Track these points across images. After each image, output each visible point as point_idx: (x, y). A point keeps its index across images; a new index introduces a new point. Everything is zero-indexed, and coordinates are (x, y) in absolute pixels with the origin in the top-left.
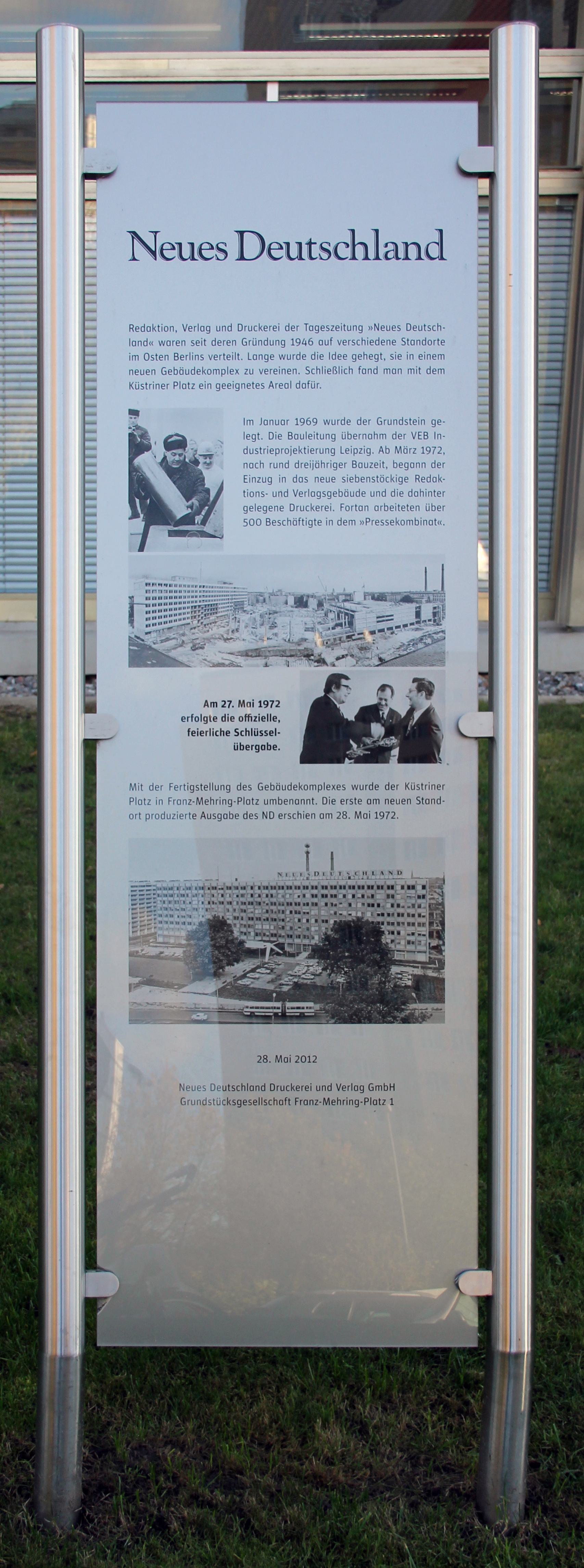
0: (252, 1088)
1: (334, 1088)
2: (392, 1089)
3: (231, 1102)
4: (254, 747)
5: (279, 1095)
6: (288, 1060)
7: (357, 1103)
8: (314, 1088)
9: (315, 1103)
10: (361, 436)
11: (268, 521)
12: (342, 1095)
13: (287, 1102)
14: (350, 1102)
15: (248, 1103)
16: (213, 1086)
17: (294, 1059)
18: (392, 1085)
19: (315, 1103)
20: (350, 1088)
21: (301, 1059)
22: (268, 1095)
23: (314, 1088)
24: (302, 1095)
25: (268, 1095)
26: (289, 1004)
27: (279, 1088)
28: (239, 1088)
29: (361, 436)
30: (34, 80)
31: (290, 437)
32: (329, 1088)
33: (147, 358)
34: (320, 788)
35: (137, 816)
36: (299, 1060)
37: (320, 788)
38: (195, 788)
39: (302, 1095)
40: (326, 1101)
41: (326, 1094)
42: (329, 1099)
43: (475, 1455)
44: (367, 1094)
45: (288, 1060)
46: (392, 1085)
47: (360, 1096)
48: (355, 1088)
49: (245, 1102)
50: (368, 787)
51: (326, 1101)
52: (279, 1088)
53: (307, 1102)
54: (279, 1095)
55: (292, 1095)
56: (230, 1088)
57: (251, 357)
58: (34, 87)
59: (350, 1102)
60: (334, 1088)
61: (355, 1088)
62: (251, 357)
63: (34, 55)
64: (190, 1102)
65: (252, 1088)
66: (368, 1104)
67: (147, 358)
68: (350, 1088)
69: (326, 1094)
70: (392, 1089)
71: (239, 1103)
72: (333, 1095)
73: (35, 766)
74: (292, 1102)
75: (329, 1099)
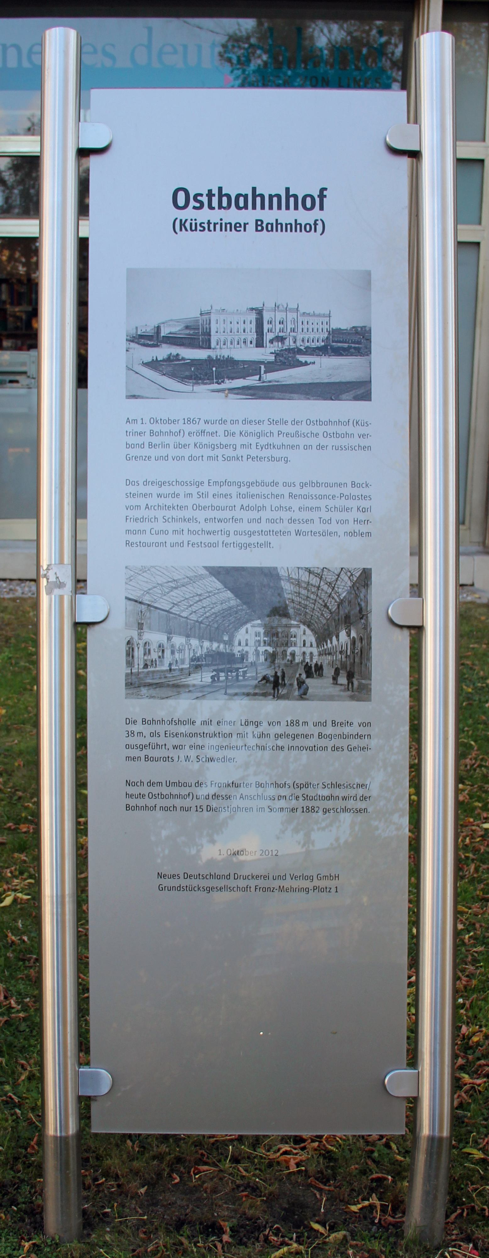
0: (218, 877)
1: (288, 877)
2: (337, 878)
3: (201, 889)
4: (231, 446)
5: (242, 883)
7: (307, 890)
11: (147, 758)
12: (295, 884)
13: (248, 889)
16: (186, 875)
18: (337, 876)
20: (301, 878)
27: (242, 877)
31: (144, 723)
33: (308, 423)
34: (259, 509)
37: (259, 509)
38: (216, 447)
42: (283, 887)
43: (406, 1184)
44: (316, 883)
46: (337, 876)
48: (306, 878)
49: (212, 888)
51: (281, 889)
52: (242, 877)
56: (201, 876)
57: (273, 509)
60: (288, 877)
61: (306, 878)
62: (273, 509)
64: (166, 888)
66: (316, 891)
67: (308, 423)
68: (301, 878)
70: (337, 878)
71: (208, 889)
72: (287, 883)
74: (253, 889)
75: (283, 887)
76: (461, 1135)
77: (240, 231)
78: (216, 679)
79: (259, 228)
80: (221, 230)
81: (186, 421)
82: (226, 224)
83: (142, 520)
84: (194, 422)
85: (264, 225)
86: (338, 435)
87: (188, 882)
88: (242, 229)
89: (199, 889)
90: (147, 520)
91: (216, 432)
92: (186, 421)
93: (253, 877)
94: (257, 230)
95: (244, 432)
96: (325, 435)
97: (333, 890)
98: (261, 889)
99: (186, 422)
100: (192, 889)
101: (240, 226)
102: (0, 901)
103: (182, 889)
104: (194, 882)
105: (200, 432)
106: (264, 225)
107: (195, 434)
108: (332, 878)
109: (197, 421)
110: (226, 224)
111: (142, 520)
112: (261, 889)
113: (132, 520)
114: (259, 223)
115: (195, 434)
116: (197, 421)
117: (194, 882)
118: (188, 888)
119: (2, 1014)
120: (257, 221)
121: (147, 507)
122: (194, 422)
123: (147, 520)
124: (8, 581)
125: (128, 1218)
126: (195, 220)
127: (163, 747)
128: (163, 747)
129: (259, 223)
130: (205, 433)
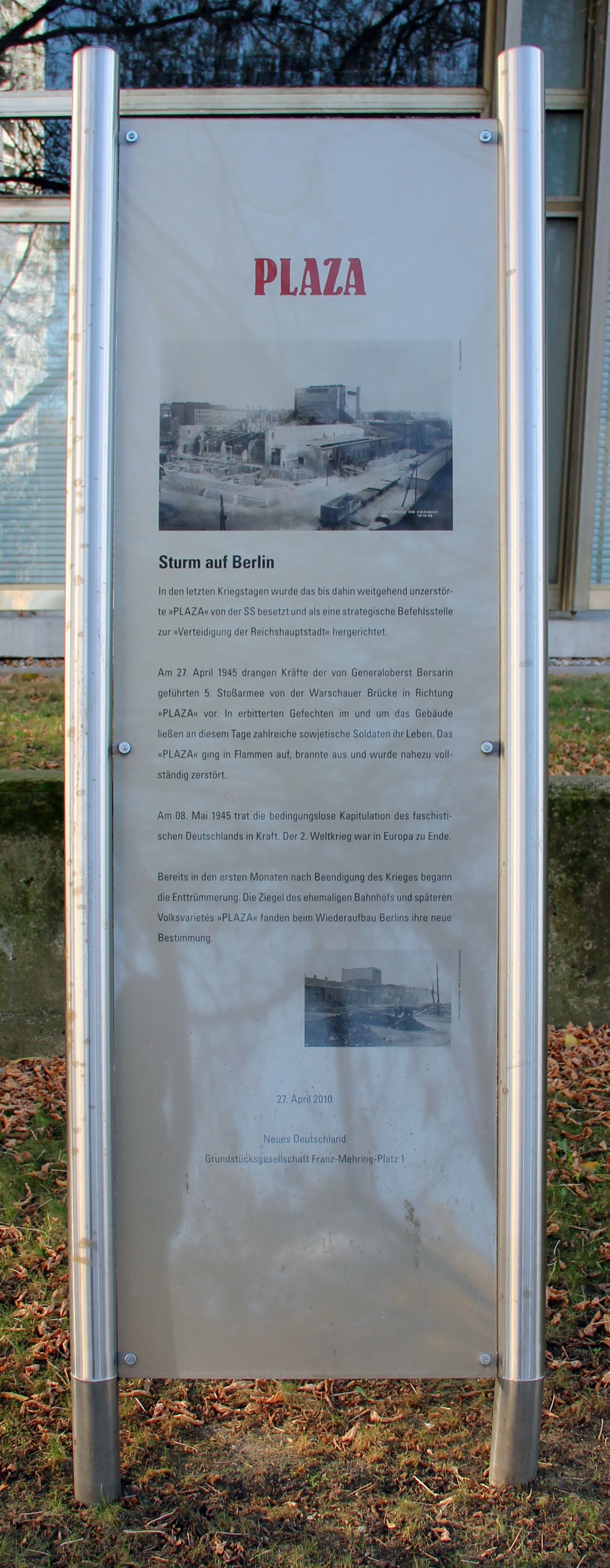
66: (381, 1161)
76: (458, 1516)
77: (249, 567)
78: (589, 1329)
79: (237, 564)
80: (259, 566)
82: (268, 561)
85: (242, 562)
88: (251, 565)
94: (234, 567)
95: (345, 814)
101: (249, 562)
102: (2, 431)
106: (242, 562)
110: (268, 561)
114: (237, 559)
120: (234, 557)
121: (228, 714)
126: (264, 556)
127: (221, 775)
128: (221, 775)
129: (237, 559)
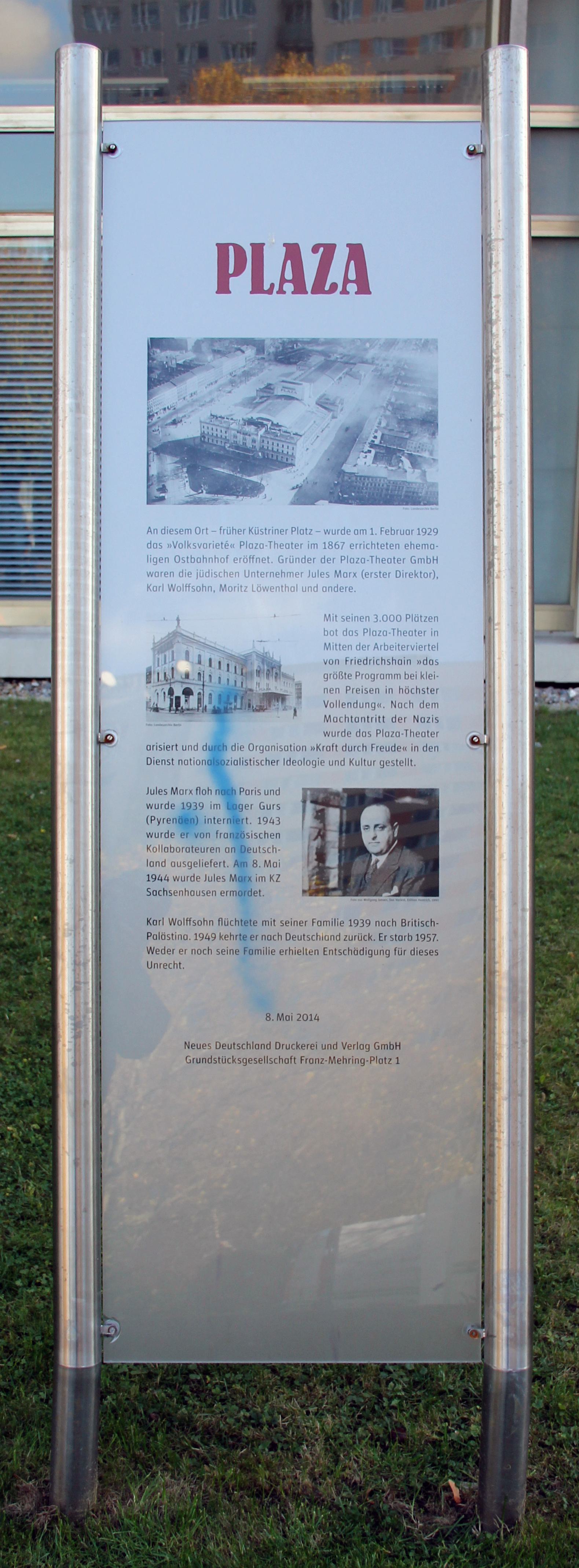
0: (258, 1047)
1: (340, 1046)
3: (236, 1061)
5: (285, 1054)
6: (289, 1018)
8: (319, 1047)
9: (320, 1061)
10: (269, 574)
12: (347, 1054)
13: (293, 1060)
14: (356, 1061)
15: (253, 1061)
17: (295, 1017)
19: (320, 1061)
20: (356, 1046)
21: (302, 1017)
22: (273, 1053)
23: (319, 1047)
24: (307, 1053)
25: (273, 1053)
26: (66, 1001)
28: (245, 1047)
29: (269, 574)
30: (53, 130)
32: (334, 1046)
35: (174, 747)
36: (301, 1019)
39: (307, 1053)
40: (332, 1060)
41: (331, 1053)
44: (373, 1052)
45: (289, 1018)
47: (362, 1054)
48: (360, 1046)
50: (189, 878)
51: (332, 1060)
53: (312, 1061)
54: (285, 1054)
55: (298, 1054)
58: (52, 136)
59: (356, 1061)
60: (340, 1046)
63: (53, 108)
65: (258, 1047)
68: (356, 1046)
69: (331, 1053)
70: (398, 1047)
72: (340, 1053)
73: (184, 92)
74: (298, 1060)
81: (327, 545)
83: (365, 662)
84: (337, 547)
86: (193, 560)
87: (221, 1053)
89: (234, 1061)
90: (372, 662)
91: (268, 558)
92: (327, 545)
93: (297, 1046)
96: (177, 560)
97: (394, 1061)
98: (308, 1061)
99: (327, 547)
100: (226, 1061)
103: (213, 1061)
104: (228, 1053)
105: (248, 557)
107: (242, 560)
108: (392, 1047)
109: (341, 545)
111: (365, 662)
112: (308, 1061)
113: (353, 662)
115: (242, 560)
116: (341, 545)
117: (228, 1053)
118: (221, 1060)
119: (2, 1337)
121: (376, 646)
122: (337, 547)
123: (372, 662)
124: (14, 681)
125: (31, 1450)
130: (255, 560)
